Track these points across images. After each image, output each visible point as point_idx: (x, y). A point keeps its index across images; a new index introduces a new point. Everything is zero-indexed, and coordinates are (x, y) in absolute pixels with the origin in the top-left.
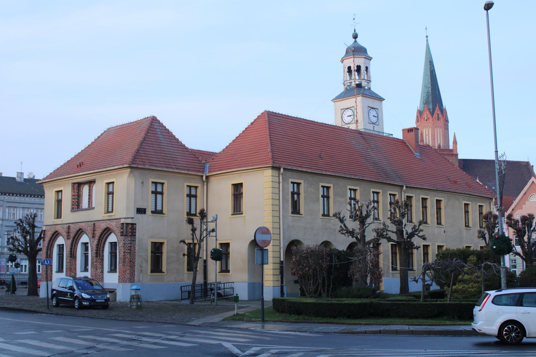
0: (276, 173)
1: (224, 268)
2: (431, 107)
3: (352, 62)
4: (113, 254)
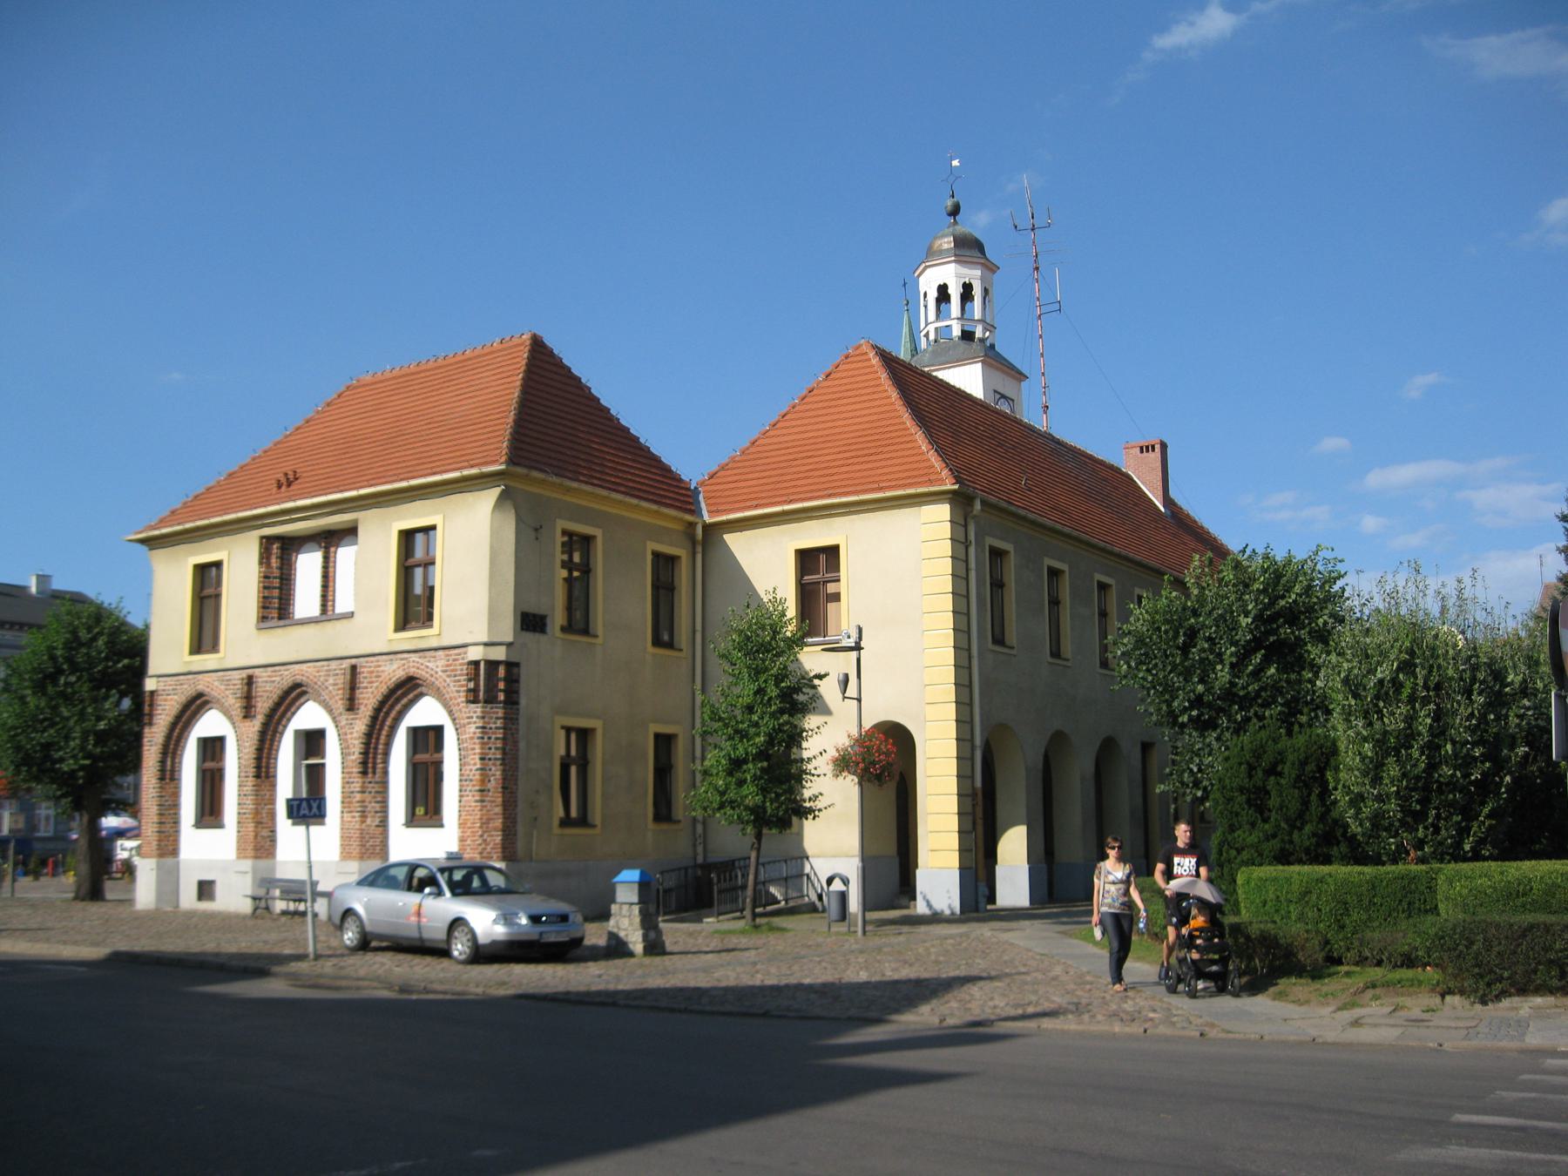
4: (211, 783)
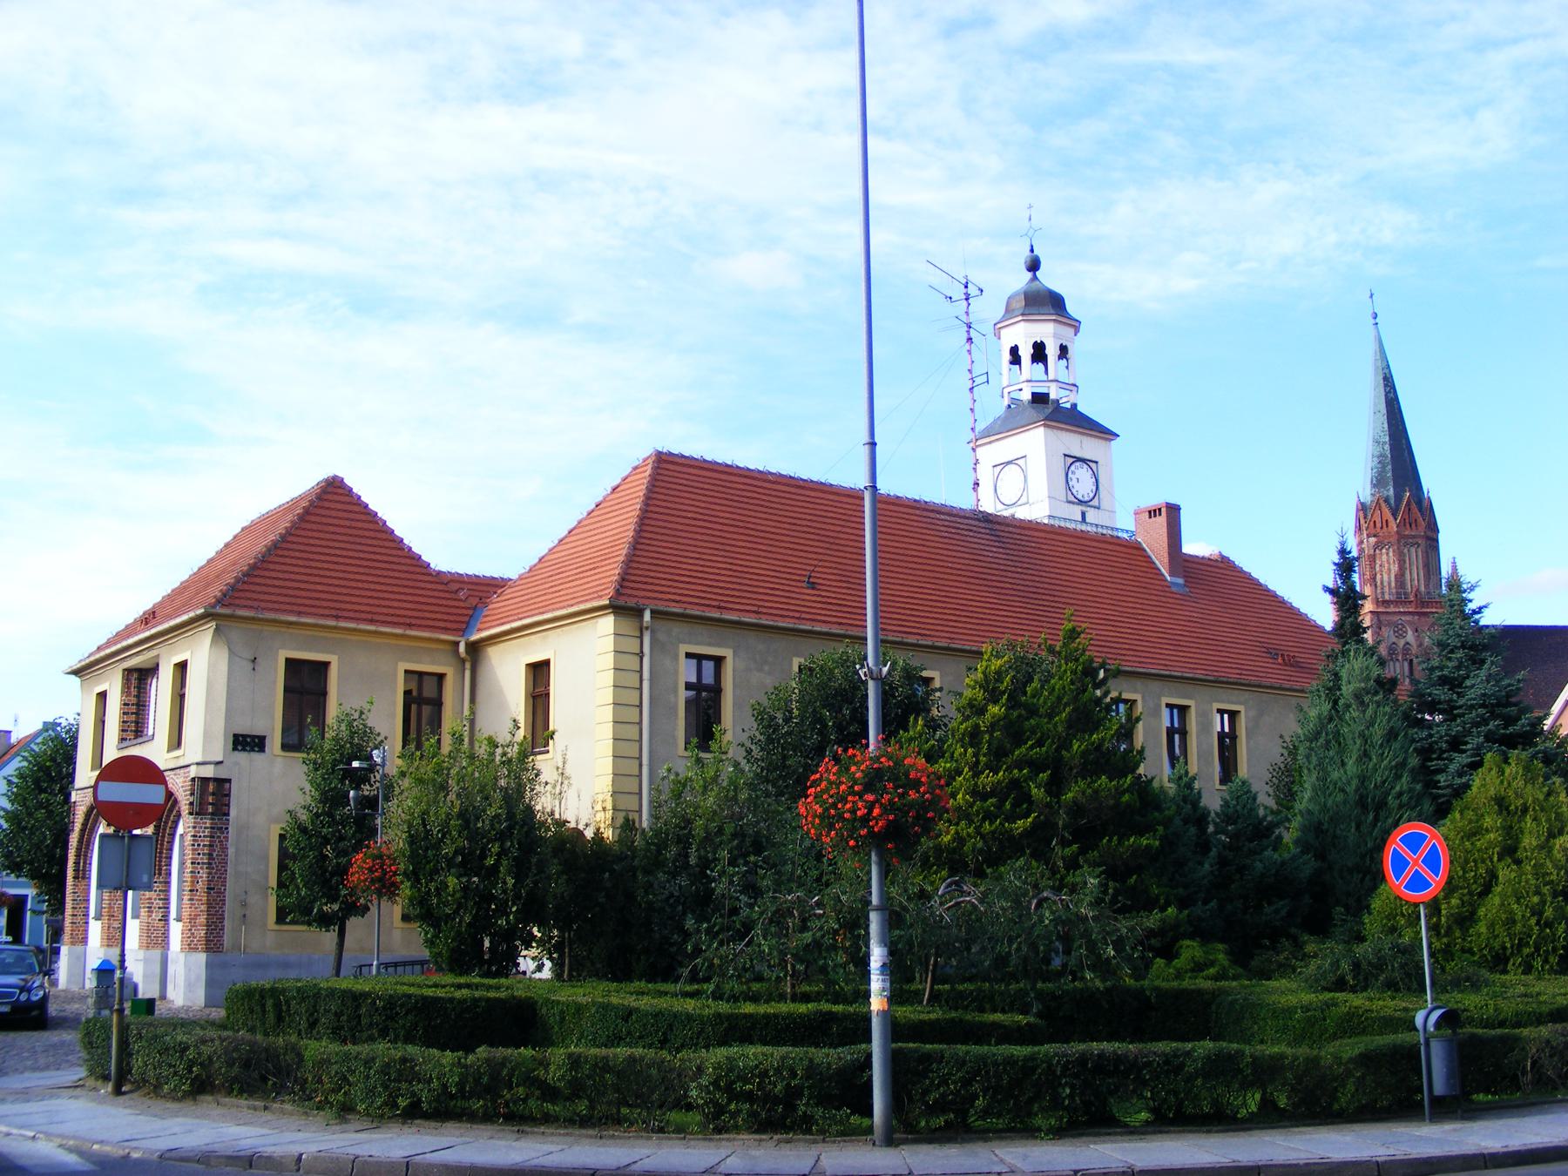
0: (629, 626)
2: (1391, 492)
3: (1023, 334)
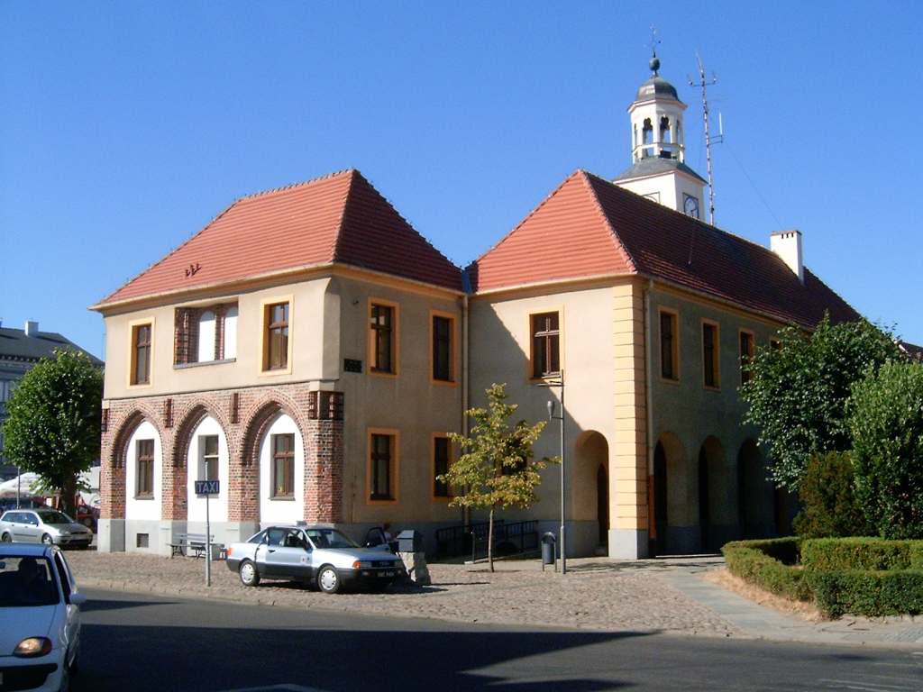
1: (382, 490)
4: (145, 468)
